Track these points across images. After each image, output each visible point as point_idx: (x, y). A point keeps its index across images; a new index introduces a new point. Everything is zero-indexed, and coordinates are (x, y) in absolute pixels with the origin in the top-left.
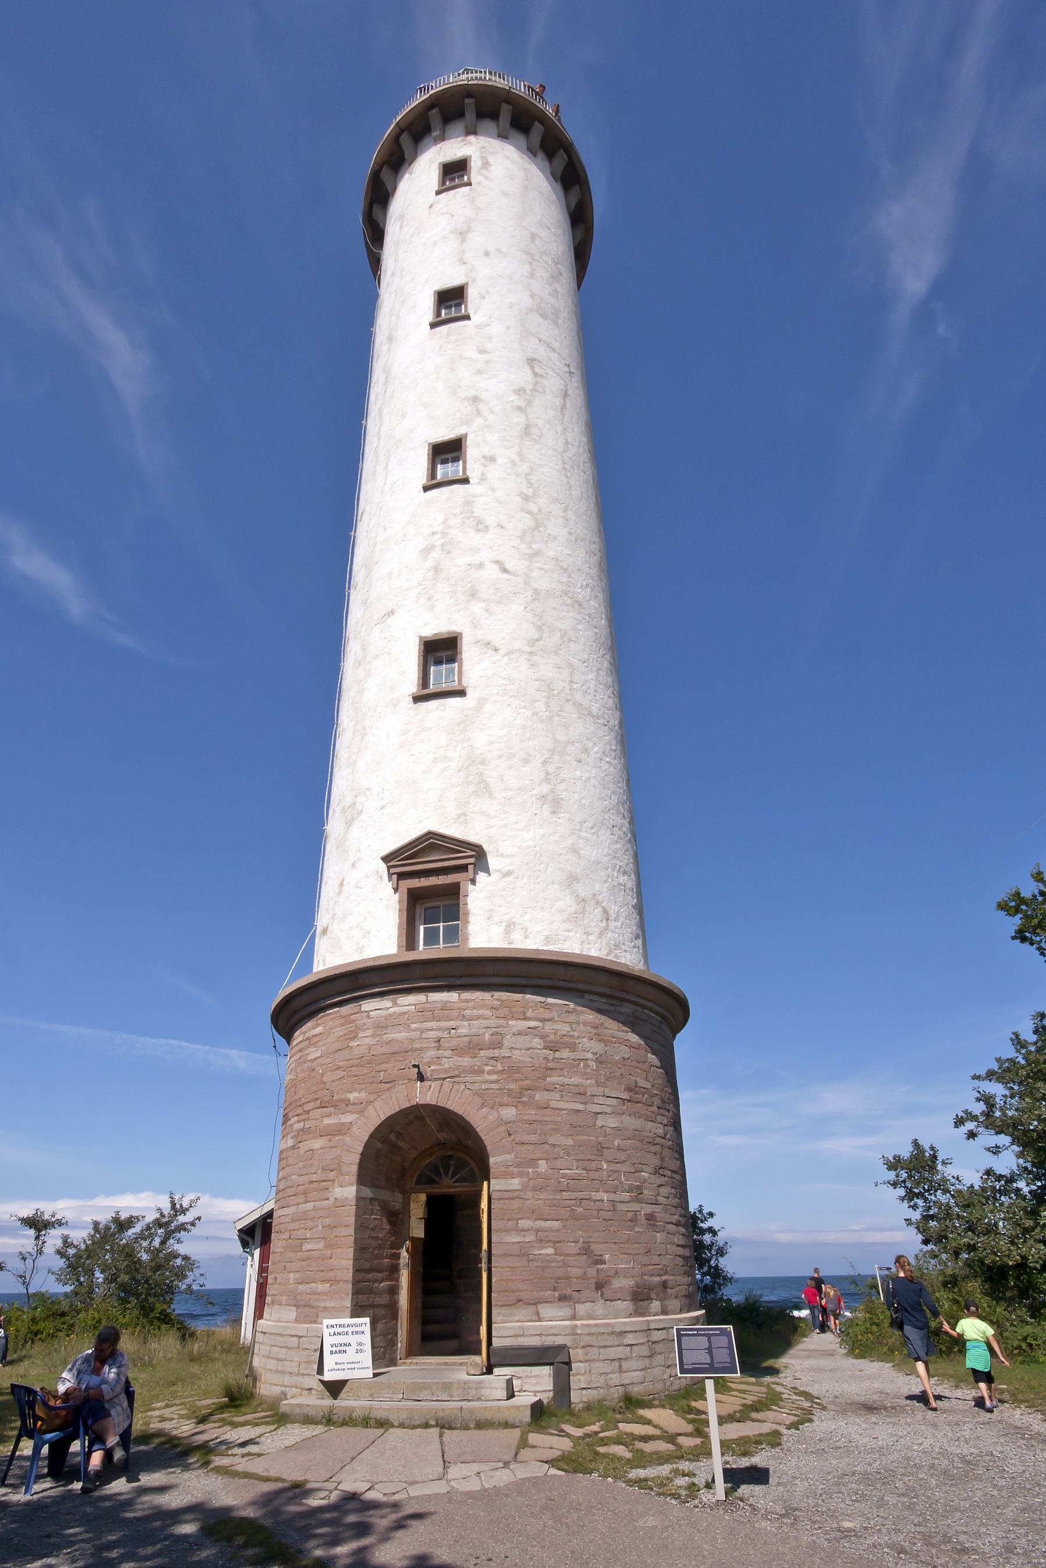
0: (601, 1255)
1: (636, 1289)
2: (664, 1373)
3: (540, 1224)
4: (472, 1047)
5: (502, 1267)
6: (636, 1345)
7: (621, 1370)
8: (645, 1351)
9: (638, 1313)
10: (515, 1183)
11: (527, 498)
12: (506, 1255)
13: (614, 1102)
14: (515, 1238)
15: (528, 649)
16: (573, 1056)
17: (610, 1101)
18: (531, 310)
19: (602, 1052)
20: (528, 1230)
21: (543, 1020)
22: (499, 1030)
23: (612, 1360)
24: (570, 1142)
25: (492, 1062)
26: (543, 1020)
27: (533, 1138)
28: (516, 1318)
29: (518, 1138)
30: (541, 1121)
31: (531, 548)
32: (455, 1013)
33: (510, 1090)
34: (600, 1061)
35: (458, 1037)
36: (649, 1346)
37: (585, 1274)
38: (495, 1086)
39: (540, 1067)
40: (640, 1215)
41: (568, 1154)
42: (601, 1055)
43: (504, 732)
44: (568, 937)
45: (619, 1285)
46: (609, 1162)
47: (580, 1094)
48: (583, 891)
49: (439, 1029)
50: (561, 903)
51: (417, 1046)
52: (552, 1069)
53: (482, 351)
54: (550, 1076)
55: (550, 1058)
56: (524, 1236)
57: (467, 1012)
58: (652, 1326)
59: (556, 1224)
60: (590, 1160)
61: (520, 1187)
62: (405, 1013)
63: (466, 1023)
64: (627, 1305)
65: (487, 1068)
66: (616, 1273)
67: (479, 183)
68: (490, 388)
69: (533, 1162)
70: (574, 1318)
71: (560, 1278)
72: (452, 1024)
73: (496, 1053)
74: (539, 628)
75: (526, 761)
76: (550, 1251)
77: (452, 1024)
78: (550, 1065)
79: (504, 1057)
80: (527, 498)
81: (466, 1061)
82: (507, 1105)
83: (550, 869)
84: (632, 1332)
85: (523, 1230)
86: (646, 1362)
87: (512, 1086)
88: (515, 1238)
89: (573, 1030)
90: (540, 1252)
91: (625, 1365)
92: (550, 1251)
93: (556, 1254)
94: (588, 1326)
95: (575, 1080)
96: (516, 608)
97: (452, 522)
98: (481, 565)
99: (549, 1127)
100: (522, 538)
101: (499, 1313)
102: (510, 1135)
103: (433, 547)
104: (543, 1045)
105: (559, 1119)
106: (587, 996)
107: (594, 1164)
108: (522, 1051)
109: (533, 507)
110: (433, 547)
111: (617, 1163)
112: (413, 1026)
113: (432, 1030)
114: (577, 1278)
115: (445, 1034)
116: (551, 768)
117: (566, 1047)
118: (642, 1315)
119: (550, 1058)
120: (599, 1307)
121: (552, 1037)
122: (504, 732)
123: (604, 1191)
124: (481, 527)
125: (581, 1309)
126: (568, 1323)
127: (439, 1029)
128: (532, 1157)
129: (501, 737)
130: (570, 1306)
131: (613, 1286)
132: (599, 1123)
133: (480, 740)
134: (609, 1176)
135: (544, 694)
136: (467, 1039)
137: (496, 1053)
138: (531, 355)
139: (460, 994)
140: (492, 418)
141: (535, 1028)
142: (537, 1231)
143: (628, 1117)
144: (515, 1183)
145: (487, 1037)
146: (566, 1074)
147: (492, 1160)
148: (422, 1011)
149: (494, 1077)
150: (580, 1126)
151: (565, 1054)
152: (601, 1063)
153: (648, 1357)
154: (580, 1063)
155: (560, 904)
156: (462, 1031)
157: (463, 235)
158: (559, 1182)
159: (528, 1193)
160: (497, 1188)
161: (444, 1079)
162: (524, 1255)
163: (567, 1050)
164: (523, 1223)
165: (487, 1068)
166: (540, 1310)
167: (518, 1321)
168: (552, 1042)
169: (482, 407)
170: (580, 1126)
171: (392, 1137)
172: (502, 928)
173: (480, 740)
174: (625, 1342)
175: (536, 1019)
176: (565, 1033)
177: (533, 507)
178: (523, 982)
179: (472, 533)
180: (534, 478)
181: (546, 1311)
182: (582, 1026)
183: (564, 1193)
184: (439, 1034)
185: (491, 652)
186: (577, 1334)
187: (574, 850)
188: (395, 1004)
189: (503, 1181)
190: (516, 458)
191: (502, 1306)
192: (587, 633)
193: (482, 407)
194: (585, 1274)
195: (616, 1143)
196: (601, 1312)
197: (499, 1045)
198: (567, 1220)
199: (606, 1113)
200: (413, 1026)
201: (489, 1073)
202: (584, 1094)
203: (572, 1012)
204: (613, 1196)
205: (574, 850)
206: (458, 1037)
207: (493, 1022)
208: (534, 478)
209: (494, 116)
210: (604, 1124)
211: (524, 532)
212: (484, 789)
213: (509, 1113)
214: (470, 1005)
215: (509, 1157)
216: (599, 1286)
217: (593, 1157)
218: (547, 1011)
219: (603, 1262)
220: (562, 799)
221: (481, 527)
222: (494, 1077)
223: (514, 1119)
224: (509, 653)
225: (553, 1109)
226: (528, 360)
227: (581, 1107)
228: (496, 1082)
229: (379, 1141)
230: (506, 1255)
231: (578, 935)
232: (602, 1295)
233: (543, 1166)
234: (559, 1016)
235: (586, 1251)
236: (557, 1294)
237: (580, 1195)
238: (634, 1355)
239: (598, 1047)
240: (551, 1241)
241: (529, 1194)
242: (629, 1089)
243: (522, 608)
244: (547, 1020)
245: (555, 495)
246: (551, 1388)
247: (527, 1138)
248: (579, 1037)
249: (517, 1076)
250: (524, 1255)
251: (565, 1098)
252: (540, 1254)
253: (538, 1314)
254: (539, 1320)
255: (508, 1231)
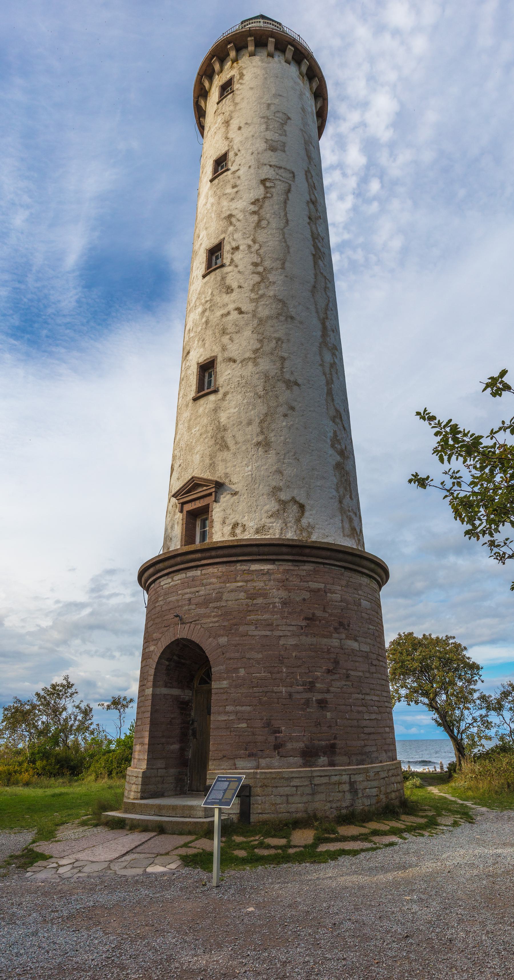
0: (279, 728)
1: (305, 749)
2: (325, 806)
3: (239, 708)
4: (206, 603)
5: (215, 736)
6: (301, 786)
7: (288, 803)
8: (308, 790)
9: (305, 765)
10: (225, 684)
11: (255, 265)
12: (218, 728)
13: (294, 628)
14: (223, 718)
15: (253, 356)
16: (265, 601)
17: (291, 628)
18: (266, 150)
19: (286, 597)
20: (231, 713)
21: (247, 581)
22: (220, 590)
23: (281, 796)
24: (260, 656)
25: (215, 610)
26: (247, 581)
27: (237, 655)
28: (222, 767)
29: (228, 655)
30: (242, 644)
31: (258, 294)
32: (198, 583)
33: (224, 626)
34: (284, 603)
35: (199, 596)
36: (312, 787)
37: (266, 740)
38: (217, 624)
39: (243, 610)
40: (312, 700)
41: (259, 664)
42: (286, 599)
43: (237, 409)
44: (272, 526)
45: (291, 747)
46: (287, 667)
47: (269, 625)
48: (283, 496)
49: (190, 593)
50: (268, 506)
51: (180, 604)
52: (250, 611)
53: (234, 187)
54: (249, 616)
55: (250, 604)
56: (229, 716)
57: (205, 581)
58: (315, 774)
59: (248, 708)
60: (274, 666)
61: (227, 686)
62: (176, 585)
63: (203, 588)
64: (298, 760)
65: (213, 614)
66: (290, 739)
67: (237, 89)
68: (237, 207)
69: (236, 670)
70: (258, 768)
71: (249, 743)
72: (197, 589)
73: (218, 604)
74: (260, 341)
75: (249, 423)
76: (244, 725)
77: (197, 589)
78: (249, 609)
79: (222, 606)
80: (255, 265)
81: (202, 611)
82: (222, 636)
83: (261, 487)
84: (298, 777)
85: (228, 713)
86: (310, 798)
87: (226, 624)
88: (223, 718)
89: (266, 585)
90: (238, 726)
91: (291, 799)
92: (244, 725)
93: (248, 727)
94: (265, 773)
95: (266, 616)
96: (247, 333)
97: (215, 293)
98: (229, 313)
99: (247, 647)
100: (252, 290)
101: (213, 764)
102: (223, 654)
103: (206, 309)
104: (246, 596)
105: (254, 642)
106: (276, 563)
107: (276, 669)
108: (233, 602)
109: (260, 269)
110: (206, 309)
111: (293, 667)
112: (179, 592)
113: (187, 594)
114: (261, 742)
115: (192, 596)
116: (265, 425)
117: (260, 597)
118: (310, 766)
119: (250, 604)
120: (276, 761)
121: (252, 591)
122: (237, 409)
123: (282, 686)
124: (229, 290)
125: (263, 762)
126: (252, 771)
127: (190, 593)
128: (235, 666)
129: (234, 413)
130: (255, 760)
131: (287, 747)
132: (281, 642)
133: (223, 417)
134: (288, 676)
135: (262, 380)
136: (203, 597)
137: (218, 604)
138: (263, 177)
139: (186, 574)
140: (238, 224)
141: (241, 586)
142: (237, 713)
143: (305, 637)
144: (225, 684)
145: (214, 595)
146: (259, 613)
147: (213, 670)
148: (185, 584)
149: (216, 619)
150: (267, 646)
151: (260, 601)
152: (285, 604)
153: (310, 794)
154: (269, 606)
155: (267, 507)
156: (202, 593)
157: (227, 123)
158: (252, 682)
159: (232, 689)
160: (214, 687)
161: (191, 622)
162: (228, 728)
163: (261, 598)
164: (229, 708)
165: (213, 614)
166: (237, 763)
167: (223, 769)
168: (251, 594)
169: (233, 220)
170: (267, 646)
171: (175, 658)
172: (231, 527)
173: (223, 417)
174: (292, 784)
175: (242, 581)
176: (260, 587)
177: (260, 269)
178: (274, 557)
179: (224, 296)
180: (262, 251)
181: (240, 763)
182: (272, 581)
183: (255, 689)
184: (190, 596)
185: (231, 363)
186: (257, 778)
187: (279, 472)
188: (173, 580)
189: (218, 682)
190: (250, 243)
191: (214, 760)
192: (297, 334)
193: (233, 220)
194: (266, 740)
195: (294, 654)
196: (277, 764)
197: (219, 599)
198: (256, 705)
199: (288, 636)
200: (179, 592)
201: (214, 617)
202: (272, 625)
203: (266, 574)
204: (289, 689)
205: (279, 472)
206: (199, 596)
207: (218, 585)
208: (262, 251)
209: (283, 51)
210: (285, 643)
211: (254, 285)
212: (224, 446)
213: (223, 640)
214: (206, 577)
215: (222, 667)
216: (277, 747)
217: (276, 665)
218: (250, 575)
219: (279, 732)
220: (271, 442)
221: (229, 290)
222: (216, 619)
223: (226, 644)
224: (241, 362)
225: (250, 636)
226: (262, 181)
227: (268, 633)
228: (217, 622)
229: (167, 661)
230: (218, 728)
231: (278, 525)
232: (278, 753)
233: (242, 672)
234: (257, 577)
235: (268, 724)
236: (247, 752)
237: (265, 689)
238: (299, 793)
239: (283, 594)
240: (245, 719)
241: (233, 690)
242: (306, 619)
243: (250, 332)
244: (249, 581)
245: (277, 256)
246: (238, 812)
247: (232, 655)
248: (270, 589)
249: (229, 617)
250: (228, 728)
251: (258, 629)
252: (238, 727)
253: (235, 765)
254: (236, 769)
255: (219, 713)
